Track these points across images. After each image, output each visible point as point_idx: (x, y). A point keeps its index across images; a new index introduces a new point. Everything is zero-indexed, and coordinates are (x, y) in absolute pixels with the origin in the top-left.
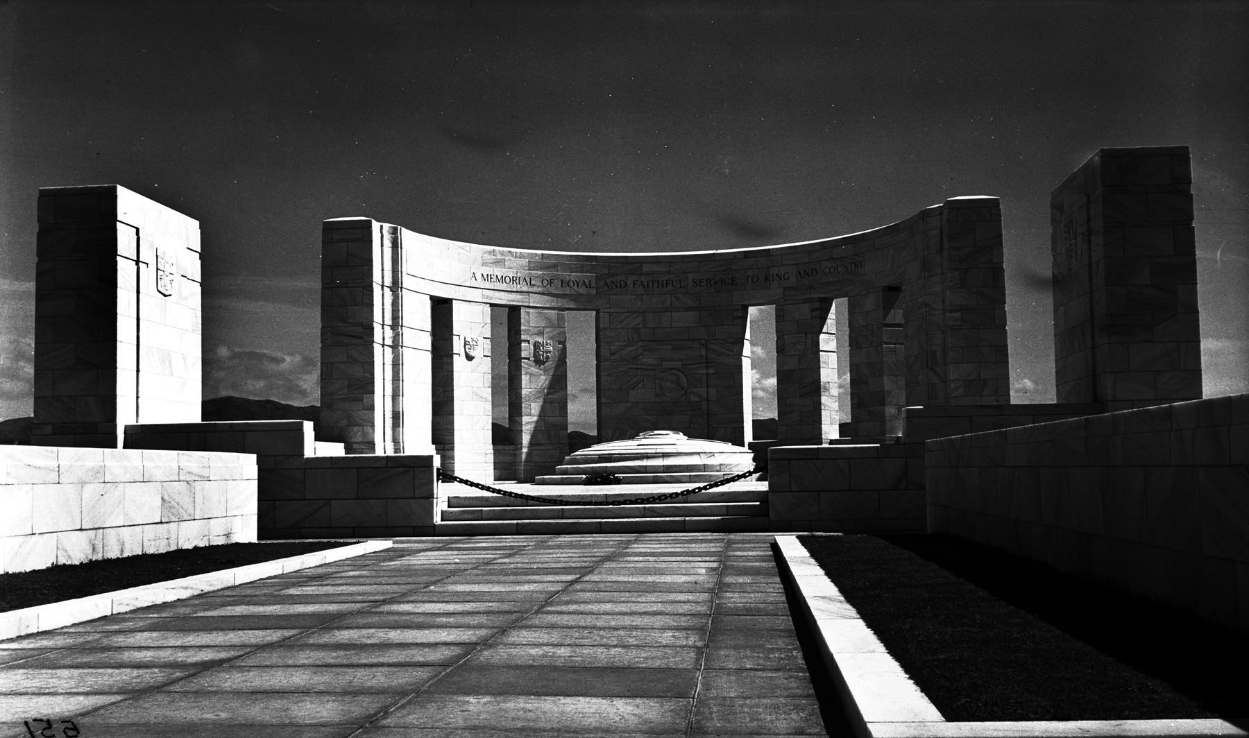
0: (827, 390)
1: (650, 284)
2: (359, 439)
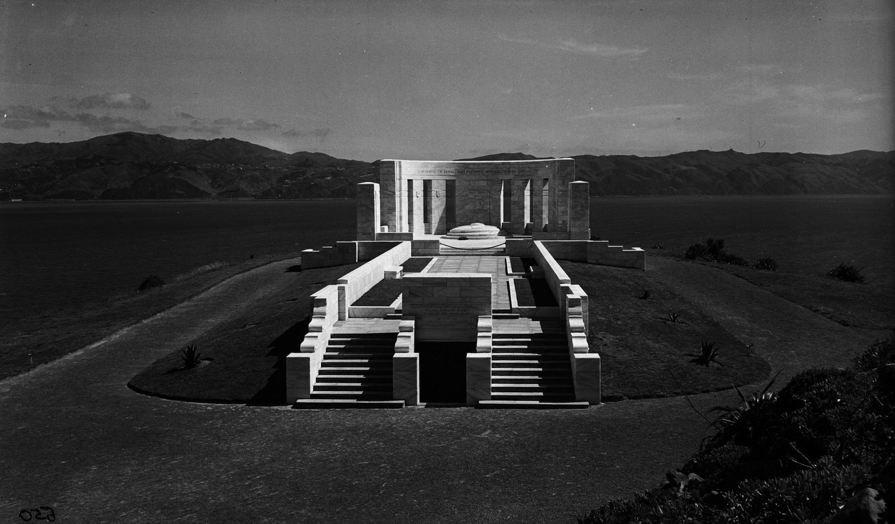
0: (526, 208)
2: (391, 225)
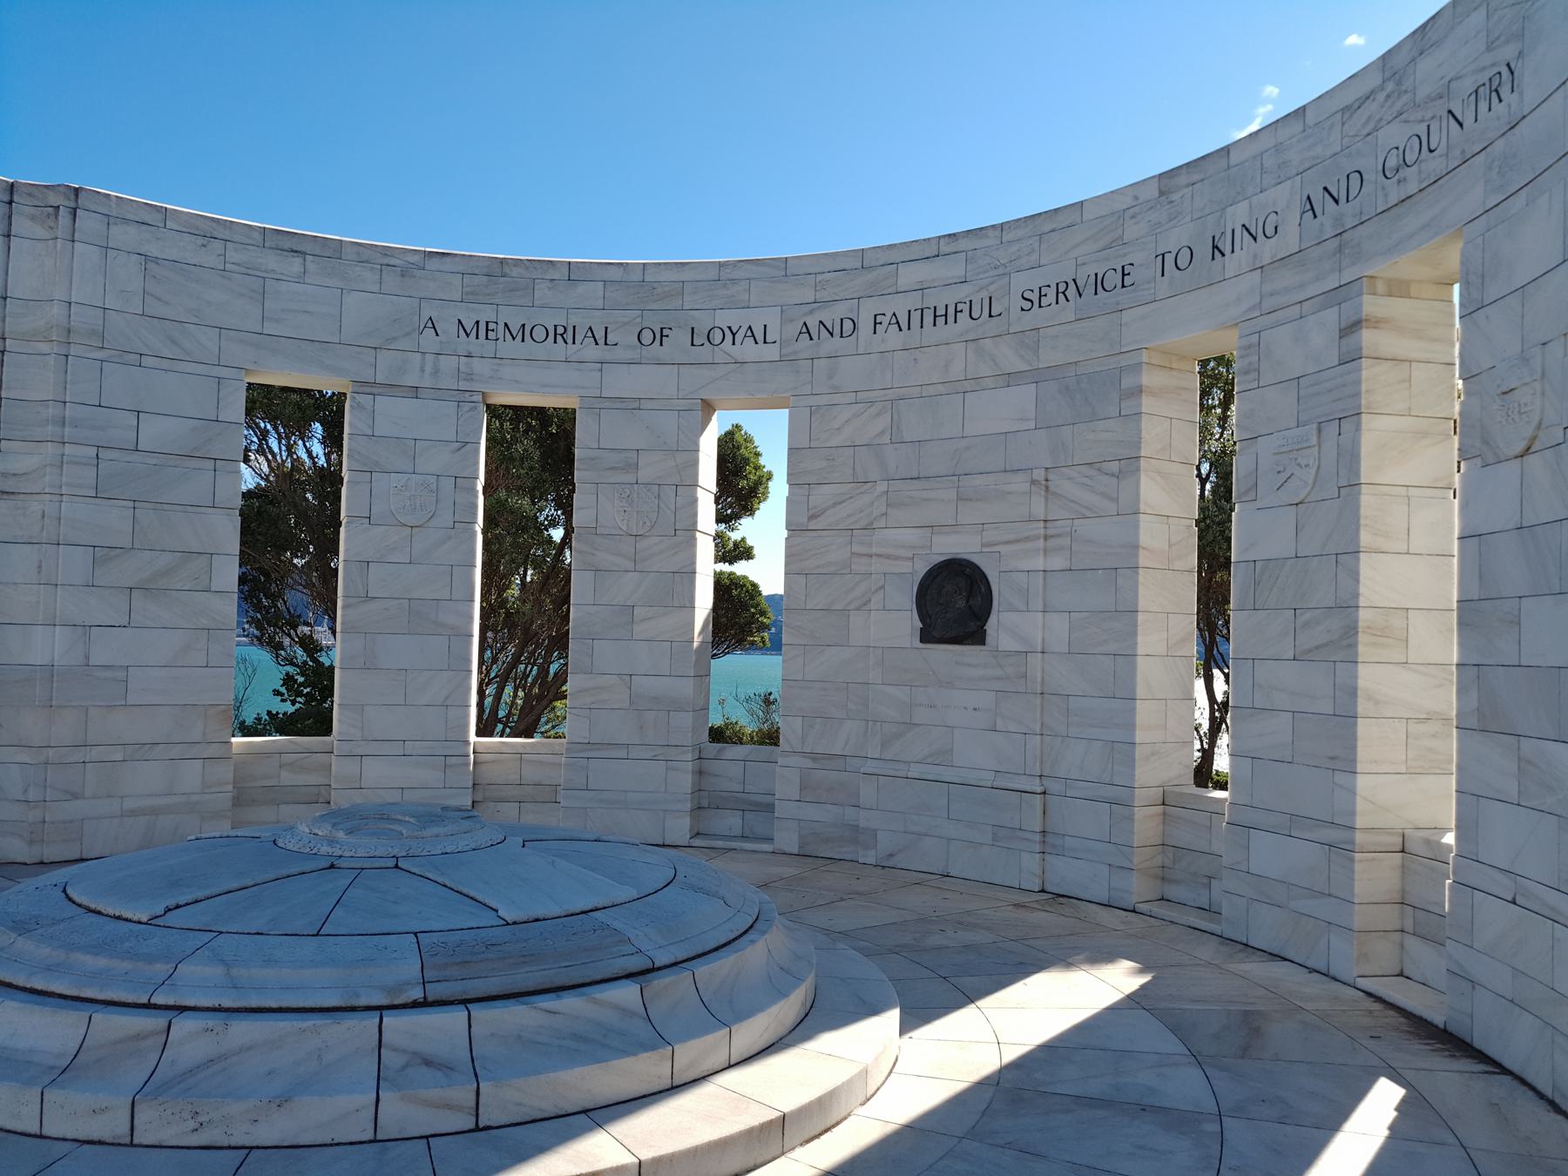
1: (916, 316)
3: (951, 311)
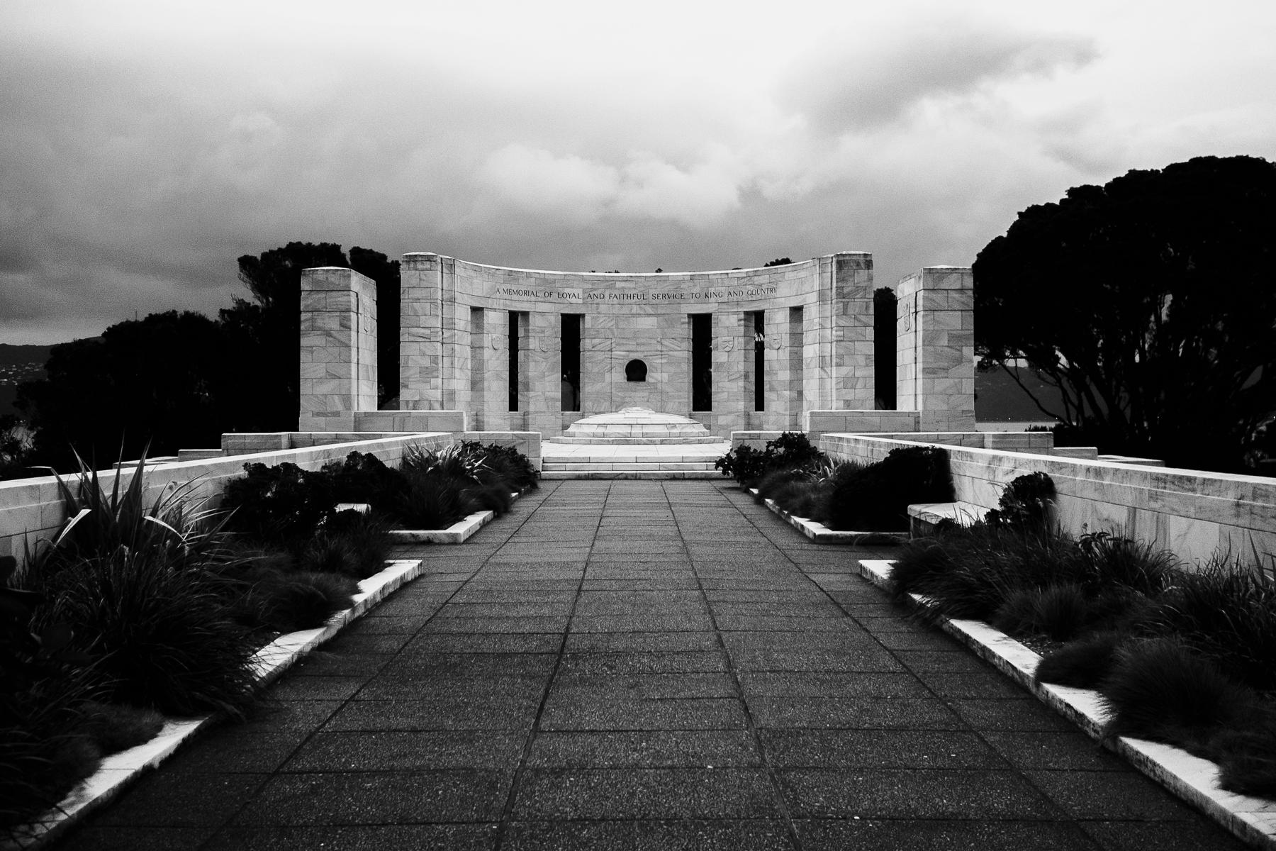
3: (632, 296)
